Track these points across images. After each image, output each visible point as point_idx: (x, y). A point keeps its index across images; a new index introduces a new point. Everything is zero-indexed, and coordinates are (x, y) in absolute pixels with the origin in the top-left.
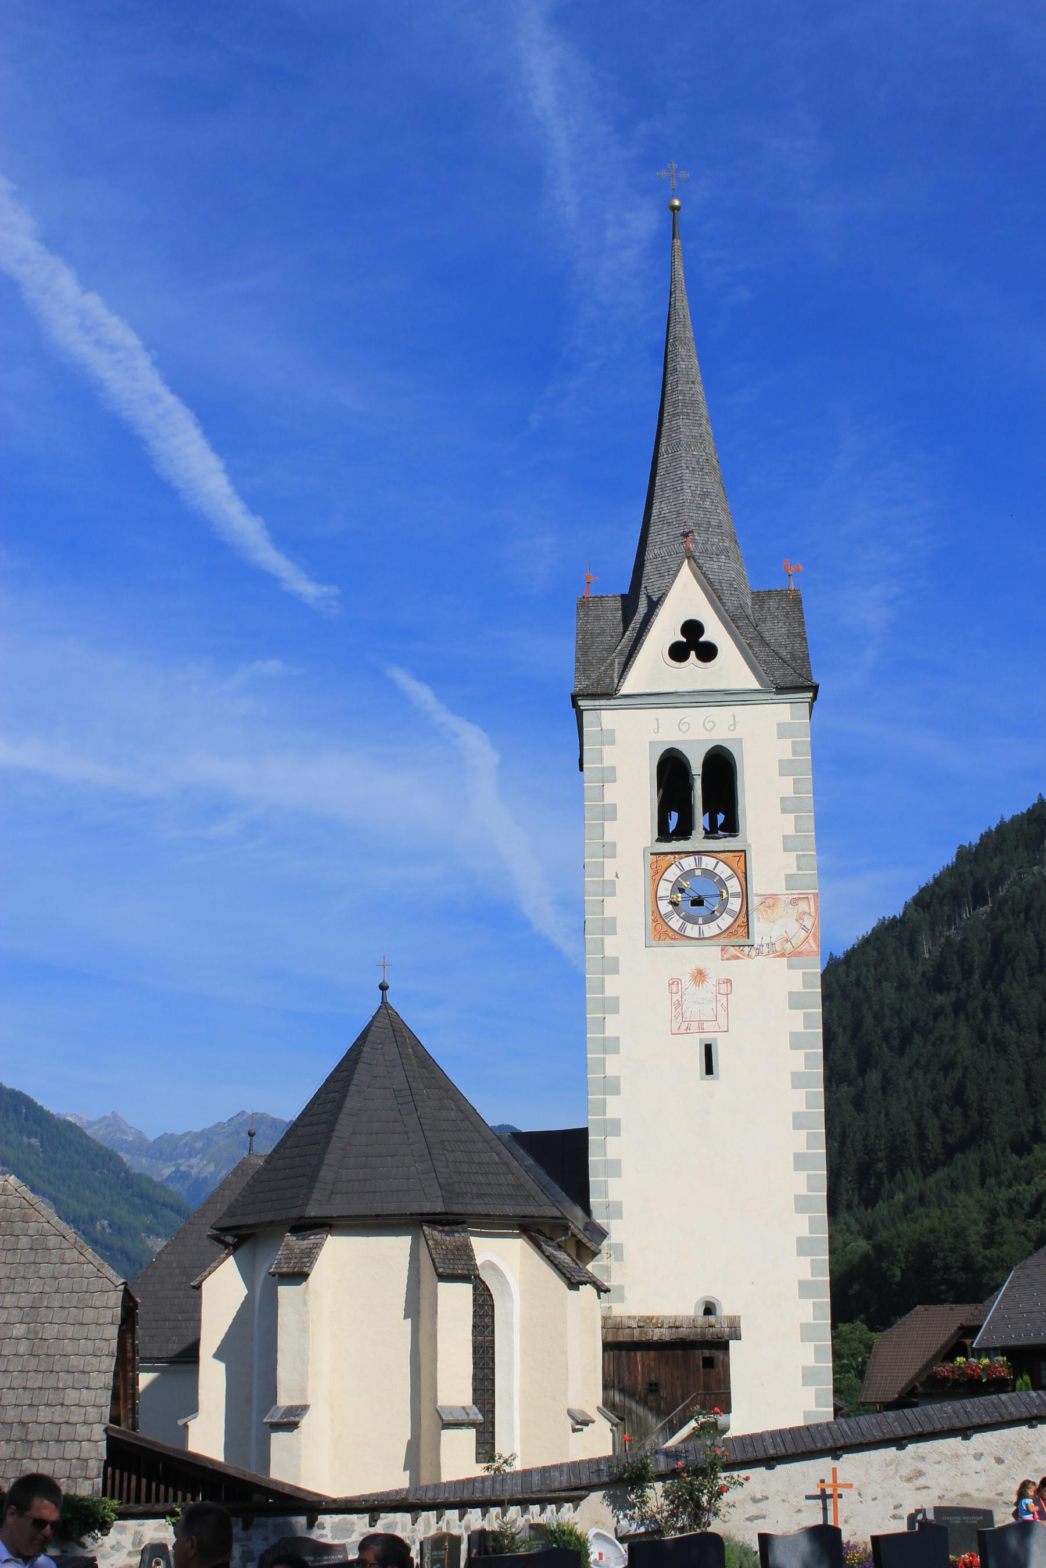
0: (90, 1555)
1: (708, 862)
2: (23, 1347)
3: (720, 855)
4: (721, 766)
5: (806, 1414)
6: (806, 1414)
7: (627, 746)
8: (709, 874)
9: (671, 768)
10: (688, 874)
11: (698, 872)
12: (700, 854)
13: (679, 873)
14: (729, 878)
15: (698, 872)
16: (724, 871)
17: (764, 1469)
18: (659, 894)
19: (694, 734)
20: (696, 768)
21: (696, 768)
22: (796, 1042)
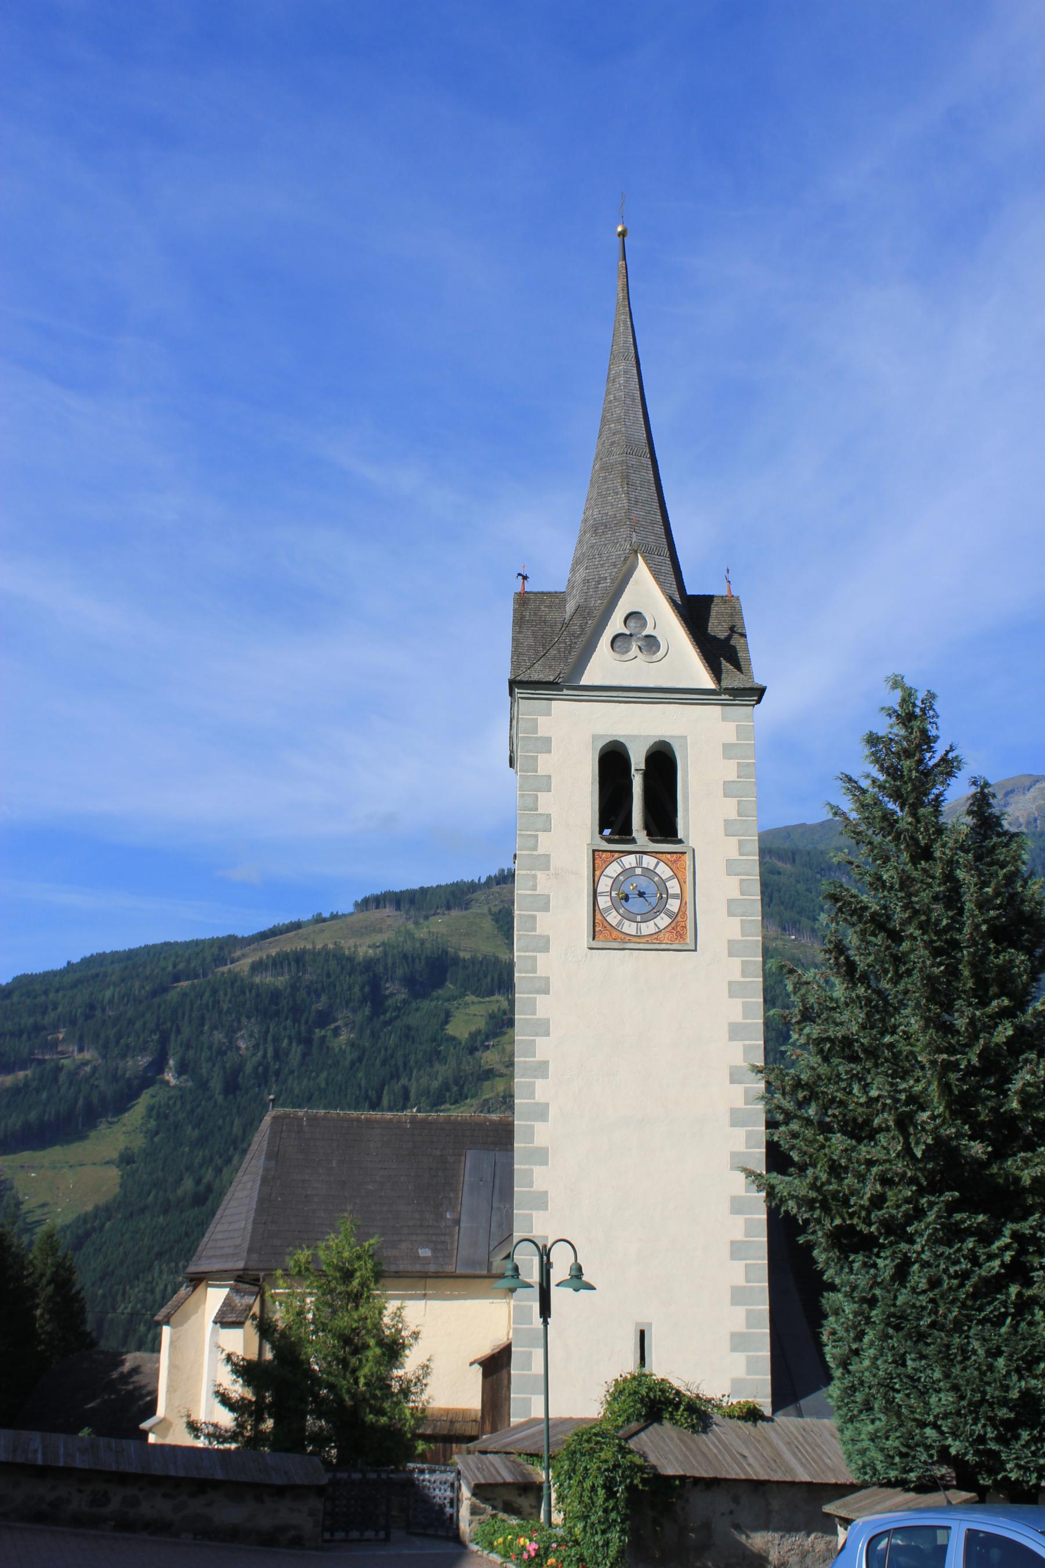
0: (474, 1499)
1: (649, 861)
2: (321, 1334)
3: (663, 857)
4: (662, 763)
5: (548, 713)
6: (548, 713)
7: (571, 736)
8: (648, 872)
9: (612, 761)
10: (628, 872)
11: (639, 871)
12: (642, 858)
13: (620, 870)
14: (670, 879)
15: (639, 871)
16: (664, 871)
17: (246, 935)
18: (599, 890)
19: (639, 727)
20: (638, 760)
21: (638, 760)
22: (734, 989)
